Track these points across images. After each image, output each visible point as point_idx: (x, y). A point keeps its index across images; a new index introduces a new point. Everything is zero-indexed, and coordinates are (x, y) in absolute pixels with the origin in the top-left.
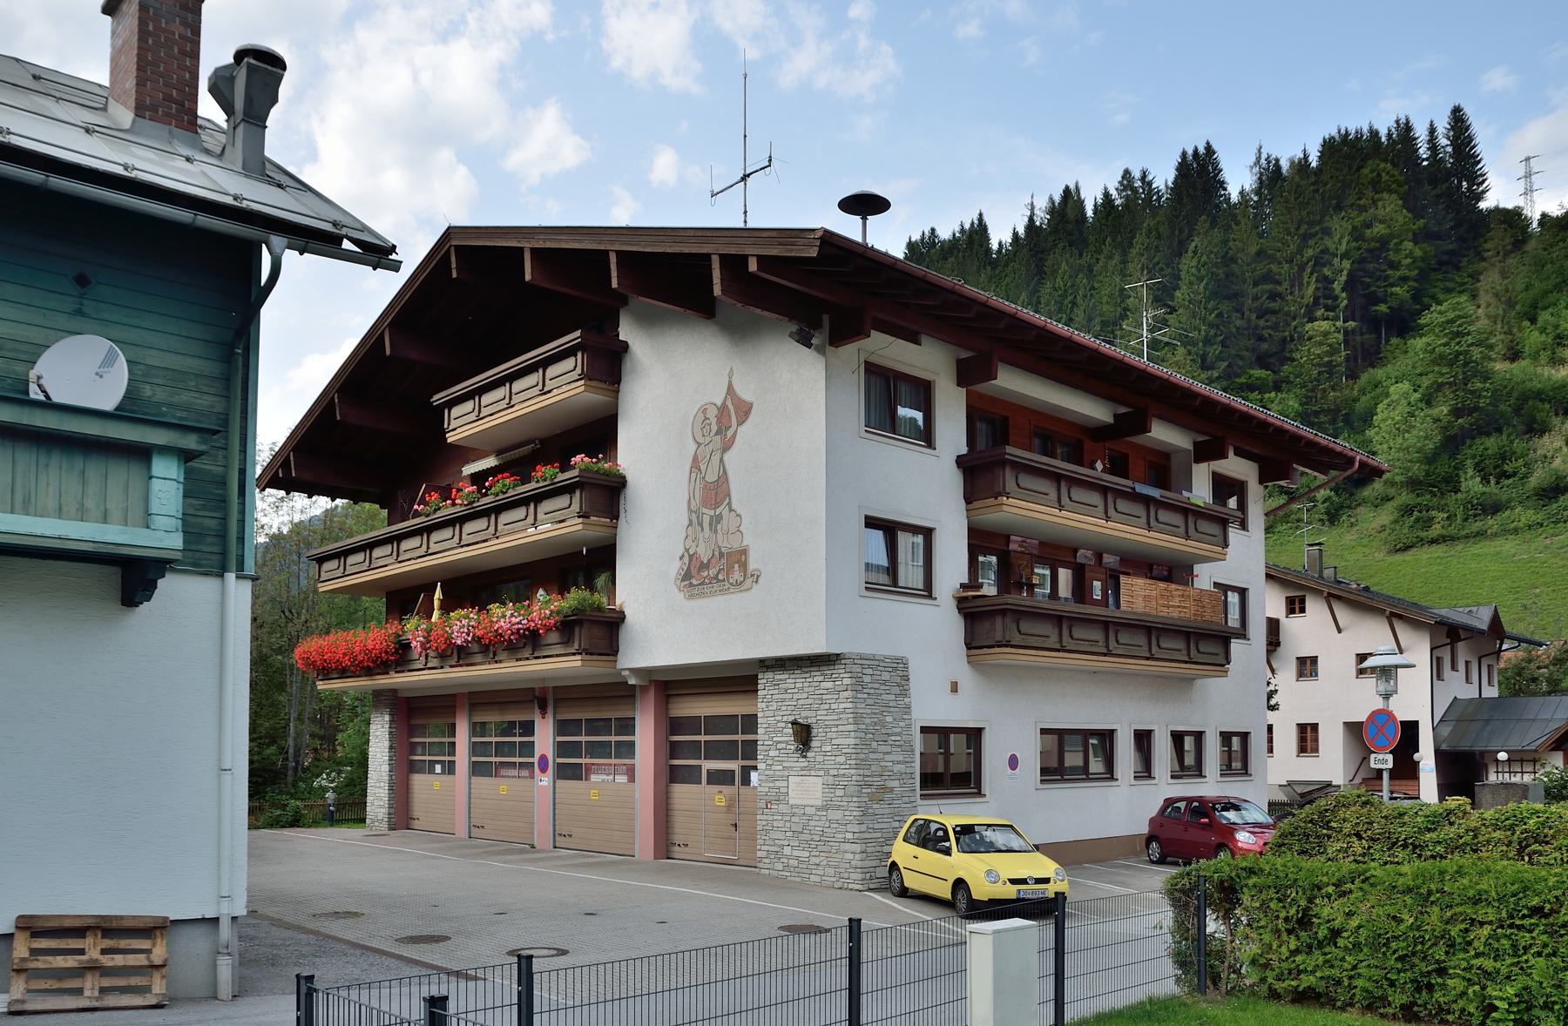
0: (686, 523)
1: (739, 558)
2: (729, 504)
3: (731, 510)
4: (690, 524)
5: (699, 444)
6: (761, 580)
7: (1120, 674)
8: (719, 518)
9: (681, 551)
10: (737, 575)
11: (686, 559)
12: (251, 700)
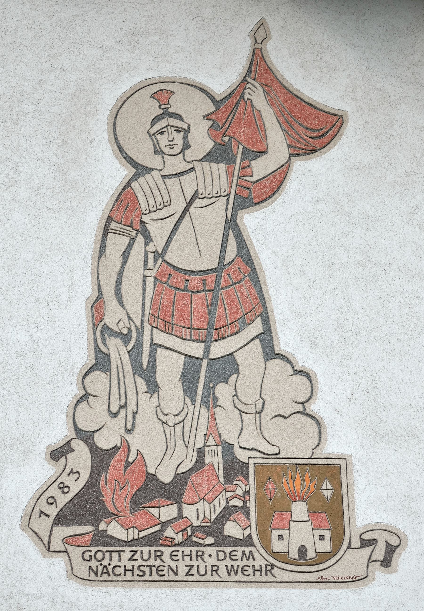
0: (83, 357)
1: (324, 485)
2: (266, 338)
3: (270, 353)
4: (101, 362)
5: (140, 170)
6: (403, 560)
7: (261, 429)
8: (226, 368)
9: (59, 432)
10: (301, 532)
11: (81, 459)
12: (70, 525)
